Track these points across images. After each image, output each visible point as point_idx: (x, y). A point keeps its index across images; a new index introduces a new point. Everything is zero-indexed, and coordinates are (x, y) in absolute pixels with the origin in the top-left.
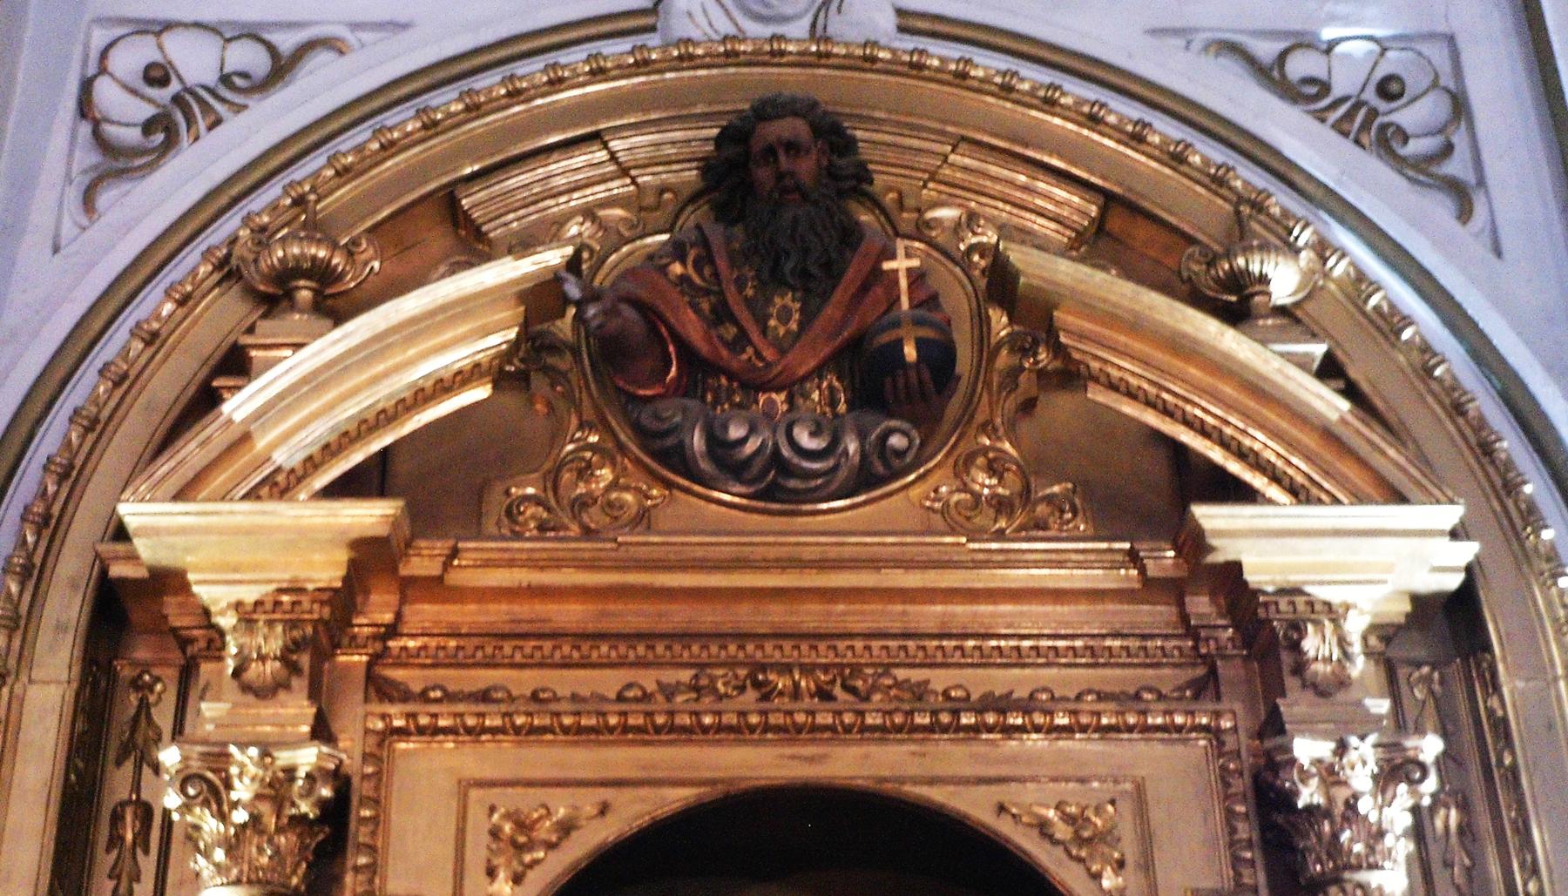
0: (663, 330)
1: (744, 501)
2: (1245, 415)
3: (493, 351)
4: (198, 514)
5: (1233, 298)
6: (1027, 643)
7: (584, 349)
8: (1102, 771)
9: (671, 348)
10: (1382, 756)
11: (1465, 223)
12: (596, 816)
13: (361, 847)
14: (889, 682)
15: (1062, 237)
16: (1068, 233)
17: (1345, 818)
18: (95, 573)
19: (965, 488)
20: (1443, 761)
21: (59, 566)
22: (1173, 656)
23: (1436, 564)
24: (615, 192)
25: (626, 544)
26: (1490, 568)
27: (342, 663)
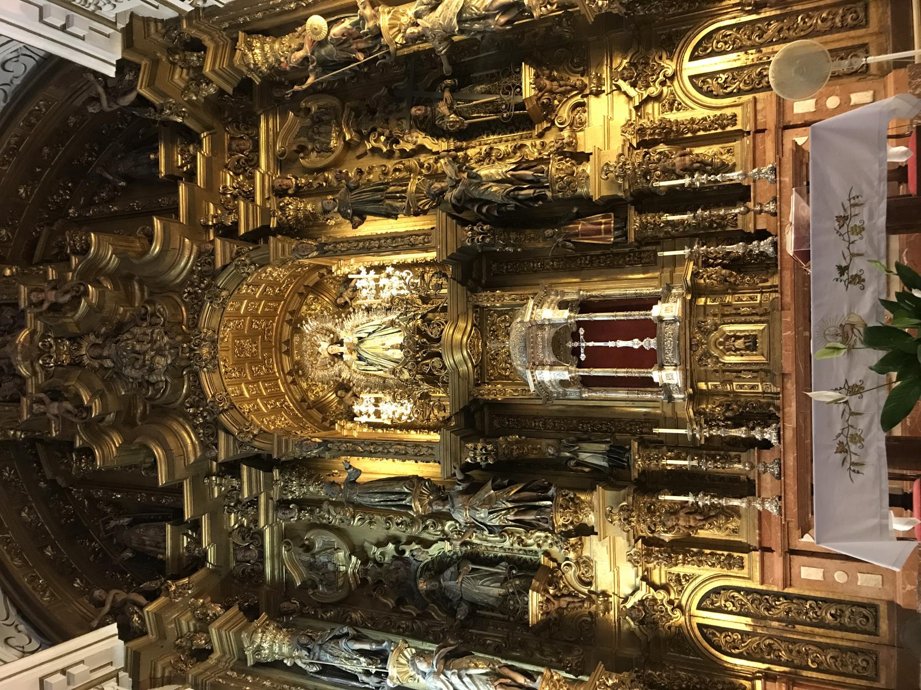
0: (393, 509)
1: (513, 524)
2: (679, 14)
4: (730, 19)
5: (68, 251)
6: (490, 545)
7: (529, 504)
8: (369, 540)
9: (183, 309)
10: (657, 367)
11: (358, 169)
12: (832, 335)
13: (914, 128)
14: (72, 242)
15: (424, 13)
16: (295, 298)
17: (782, 309)
18: (129, 654)
19: (732, 410)
20: (239, 340)
21: (792, 570)
22: (276, 309)
23: (862, 257)
24: (633, 375)
25: (430, 429)
26: (797, 537)
27: (91, 236)
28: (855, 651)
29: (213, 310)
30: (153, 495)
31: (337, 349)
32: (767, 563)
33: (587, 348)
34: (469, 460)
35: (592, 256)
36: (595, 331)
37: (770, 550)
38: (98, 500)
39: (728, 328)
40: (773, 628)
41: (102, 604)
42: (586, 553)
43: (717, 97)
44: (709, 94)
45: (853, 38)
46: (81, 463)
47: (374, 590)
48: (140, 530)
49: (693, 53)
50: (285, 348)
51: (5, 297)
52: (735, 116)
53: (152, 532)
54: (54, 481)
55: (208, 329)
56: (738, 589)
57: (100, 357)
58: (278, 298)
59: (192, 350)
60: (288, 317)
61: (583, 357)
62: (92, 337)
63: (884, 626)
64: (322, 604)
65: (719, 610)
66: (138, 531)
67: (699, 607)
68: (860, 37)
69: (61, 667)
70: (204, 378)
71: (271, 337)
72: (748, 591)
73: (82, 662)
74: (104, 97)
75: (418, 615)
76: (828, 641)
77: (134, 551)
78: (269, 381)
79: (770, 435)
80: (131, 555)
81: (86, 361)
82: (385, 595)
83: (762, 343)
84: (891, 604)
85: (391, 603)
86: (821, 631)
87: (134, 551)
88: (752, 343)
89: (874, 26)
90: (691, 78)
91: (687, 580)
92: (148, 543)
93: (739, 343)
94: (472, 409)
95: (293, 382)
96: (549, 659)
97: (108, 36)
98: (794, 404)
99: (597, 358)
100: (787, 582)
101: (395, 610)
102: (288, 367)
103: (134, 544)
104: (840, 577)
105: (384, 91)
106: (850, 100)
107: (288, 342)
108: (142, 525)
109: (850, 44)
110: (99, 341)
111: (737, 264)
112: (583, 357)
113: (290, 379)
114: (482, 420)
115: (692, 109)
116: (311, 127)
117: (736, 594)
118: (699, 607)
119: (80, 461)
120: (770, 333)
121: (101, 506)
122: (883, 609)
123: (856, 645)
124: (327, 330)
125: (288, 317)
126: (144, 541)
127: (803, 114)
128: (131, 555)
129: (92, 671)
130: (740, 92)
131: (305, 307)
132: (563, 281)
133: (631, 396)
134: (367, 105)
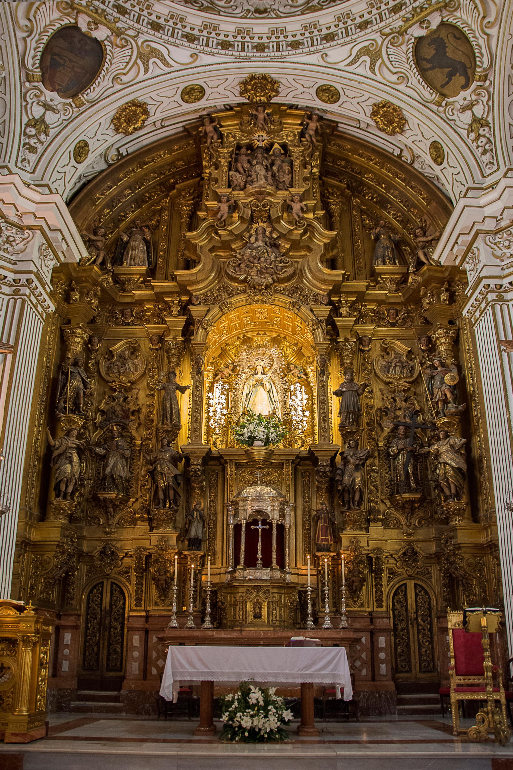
3: (179, 719)
22: (287, 330)
28: (98, 660)
29: (286, 304)
30: (165, 253)
31: (260, 370)
32: (140, 619)
33: (258, 530)
34: (192, 461)
35: (310, 530)
36: (267, 534)
37: (147, 621)
38: (160, 215)
39: (265, 604)
40: (105, 620)
41: (95, 234)
42: (139, 523)
43: (393, 598)
44: (396, 594)
45: (415, 665)
46: (186, 206)
47: (109, 397)
48: (142, 246)
49: (419, 585)
50: (261, 333)
51: (297, 178)
52: (197, 300)
53: (141, 255)
54: (174, 188)
55: (274, 300)
56: (124, 604)
57: (257, 234)
58: (294, 332)
59: (260, 291)
60: (282, 336)
61: (253, 527)
62: (269, 230)
63: (111, 674)
64: (98, 363)
65: (112, 594)
66: (141, 245)
67: (112, 583)
68: (415, 668)
69: (66, 237)
70: (243, 297)
71: (269, 325)
72: (124, 609)
73: (68, 246)
74: (425, 239)
75: (95, 423)
76: (101, 646)
77: (128, 242)
78: (240, 326)
79: (207, 624)
80: (125, 239)
81: (255, 226)
82: (106, 404)
83: (258, 621)
84: (123, 678)
85: (102, 406)
86: (106, 644)
87: (128, 242)
88: (258, 616)
89: (420, 675)
90: (405, 584)
91: (126, 577)
92: (134, 252)
93: (257, 610)
94: (222, 460)
95: (239, 338)
96: (76, 500)
97: (455, 260)
98: (226, 636)
99: (251, 535)
100: (130, 629)
101: (98, 410)
102: (249, 335)
103: (132, 243)
104: (136, 654)
105: (418, 408)
106: (383, 664)
107: (265, 334)
108: (145, 247)
109: (412, 664)
110: (267, 234)
111: (303, 606)
112: (253, 527)
113: (241, 336)
114: (215, 465)
115: (388, 585)
116: (400, 361)
117: (121, 603)
118: (112, 583)
119: (188, 206)
120: (263, 625)
121: (157, 218)
122: (122, 674)
123: (100, 660)
124: (272, 365)
125: (282, 336)
126: (135, 250)
127: (378, 641)
128: (125, 239)
129: (63, 252)
130: (394, 610)
131: (288, 344)
132: (371, 719)
133: (246, 753)
134: (410, 397)
